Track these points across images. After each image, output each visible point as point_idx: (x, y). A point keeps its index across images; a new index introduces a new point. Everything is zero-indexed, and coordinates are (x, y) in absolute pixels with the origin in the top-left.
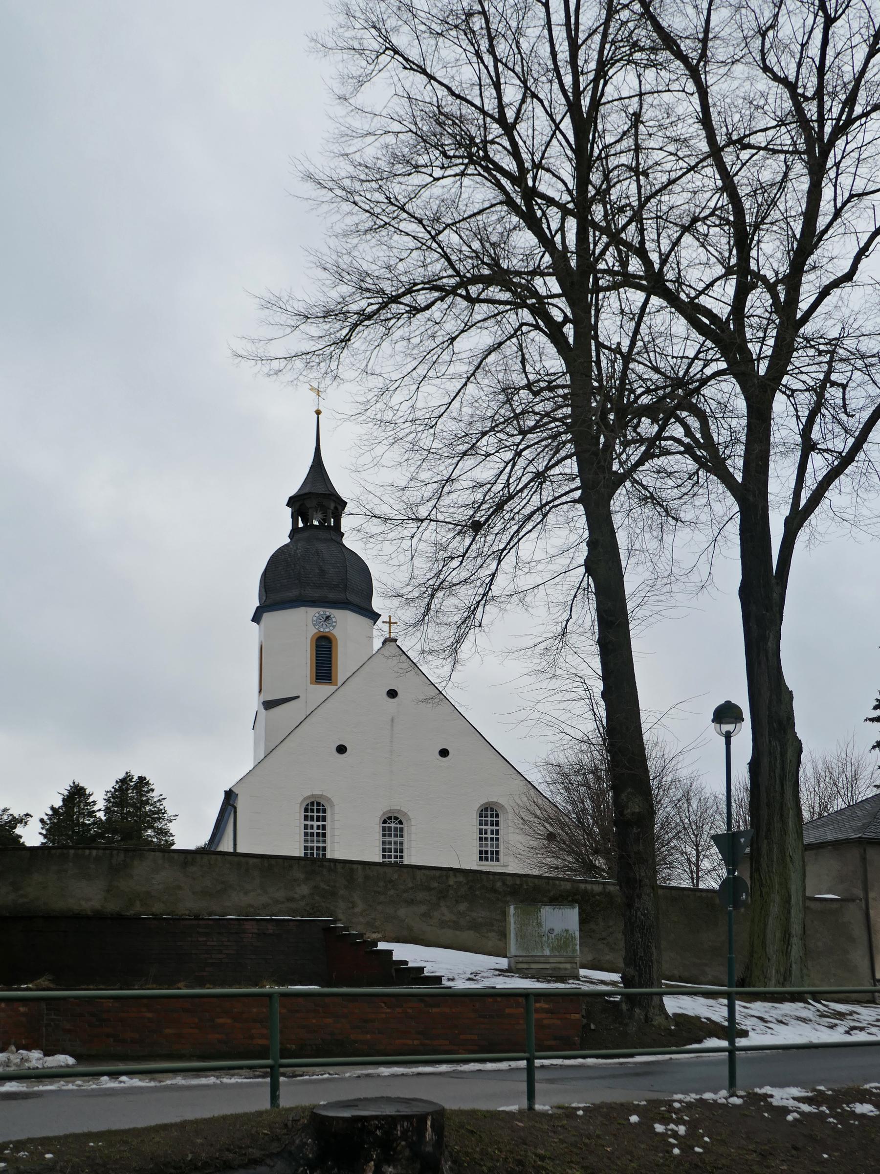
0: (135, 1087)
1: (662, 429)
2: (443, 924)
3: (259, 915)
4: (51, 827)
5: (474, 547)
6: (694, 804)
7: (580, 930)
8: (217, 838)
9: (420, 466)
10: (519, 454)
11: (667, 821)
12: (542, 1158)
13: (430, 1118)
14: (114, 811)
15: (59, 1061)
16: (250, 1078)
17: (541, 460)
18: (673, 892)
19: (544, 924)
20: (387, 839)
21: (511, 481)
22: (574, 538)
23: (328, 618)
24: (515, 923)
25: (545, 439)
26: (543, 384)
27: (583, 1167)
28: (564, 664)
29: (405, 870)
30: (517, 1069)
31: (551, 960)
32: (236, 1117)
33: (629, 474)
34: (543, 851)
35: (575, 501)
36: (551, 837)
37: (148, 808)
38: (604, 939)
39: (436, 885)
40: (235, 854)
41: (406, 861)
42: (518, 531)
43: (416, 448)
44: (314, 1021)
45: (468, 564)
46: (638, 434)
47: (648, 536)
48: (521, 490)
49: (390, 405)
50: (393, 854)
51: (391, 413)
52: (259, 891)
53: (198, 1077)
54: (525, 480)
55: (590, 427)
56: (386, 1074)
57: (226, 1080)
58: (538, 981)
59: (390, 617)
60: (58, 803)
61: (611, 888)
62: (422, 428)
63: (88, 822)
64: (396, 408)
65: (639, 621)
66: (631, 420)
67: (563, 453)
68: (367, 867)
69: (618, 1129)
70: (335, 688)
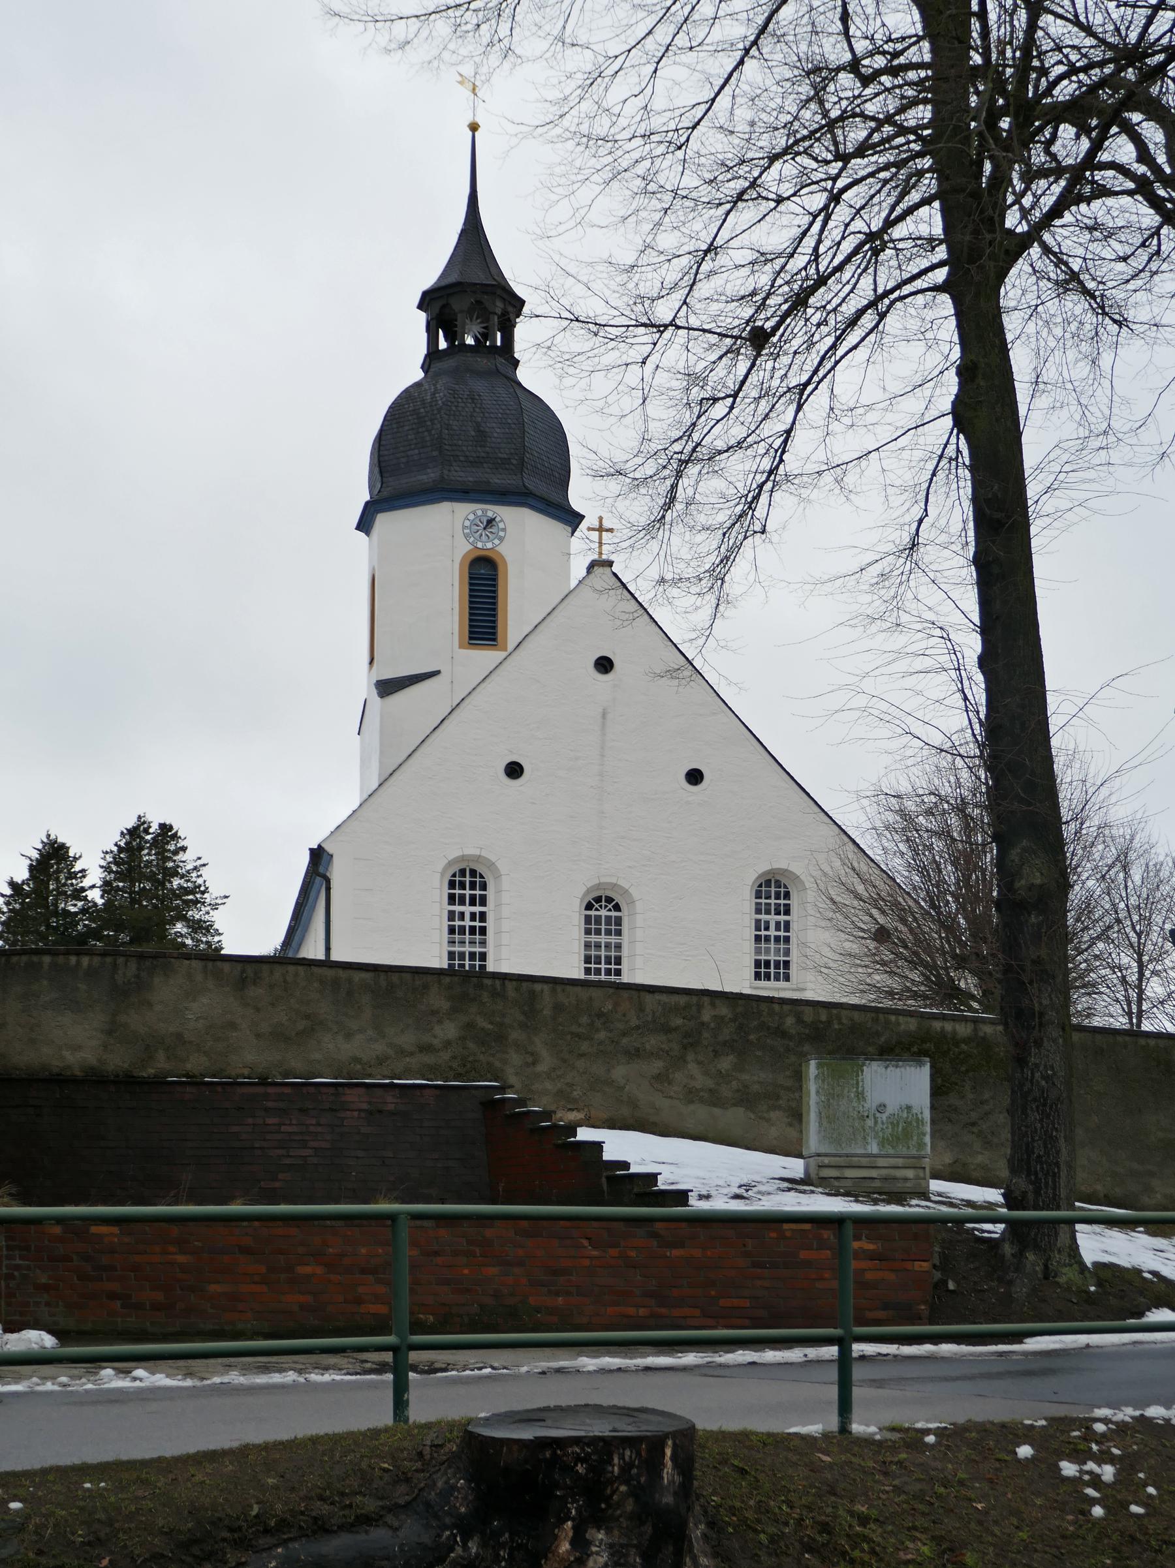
0: (159, 1388)
1: (1097, 146)
2: (691, 1095)
3: (370, 1076)
4: (9, 918)
5: (753, 379)
6: (1137, 875)
7: (933, 1107)
8: (296, 938)
9: (659, 224)
10: (835, 198)
11: (1088, 907)
12: (864, 1520)
13: (670, 1443)
14: (118, 889)
15: (30, 1341)
16: (357, 1374)
17: (876, 208)
18: (1098, 1037)
19: (868, 1094)
20: (593, 938)
21: (822, 249)
22: (934, 360)
23: (490, 522)
24: (818, 1092)
25: (886, 167)
26: (880, 62)
27: (933, 1538)
28: (914, 606)
29: (625, 994)
30: (819, 1362)
31: (881, 1162)
32: (335, 1440)
33: (1033, 235)
34: (867, 961)
35: (936, 289)
36: (882, 935)
37: (176, 882)
38: (973, 1124)
39: (679, 1021)
40: (328, 963)
41: (626, 978)
42: (834, 347)
43: (652, 187)
44: (466, 1271)
45: (745, 409)
46: (1054, 157)
47: (1071, 354)
48: (840, 268)
49: (604, 104)
50: (603, 966)
51: (606, 121)
52: (370, 1032)
53: (266, 1369)
54: (847, 246)
55: (967, 140)
56: (591, 1368)
57: (314, 1377)
58: (857, 1201)
59: (601, 519)
60: (21, 874)
61: (988, 1029)
62: (662, 149)
63: (73, 909)
64: (616, 110)
65: (1048, 520)
66: (1040, 130)
67: (915, 197)
68: (559, 988)
69: (996, 1469)
70: (503, 654)
